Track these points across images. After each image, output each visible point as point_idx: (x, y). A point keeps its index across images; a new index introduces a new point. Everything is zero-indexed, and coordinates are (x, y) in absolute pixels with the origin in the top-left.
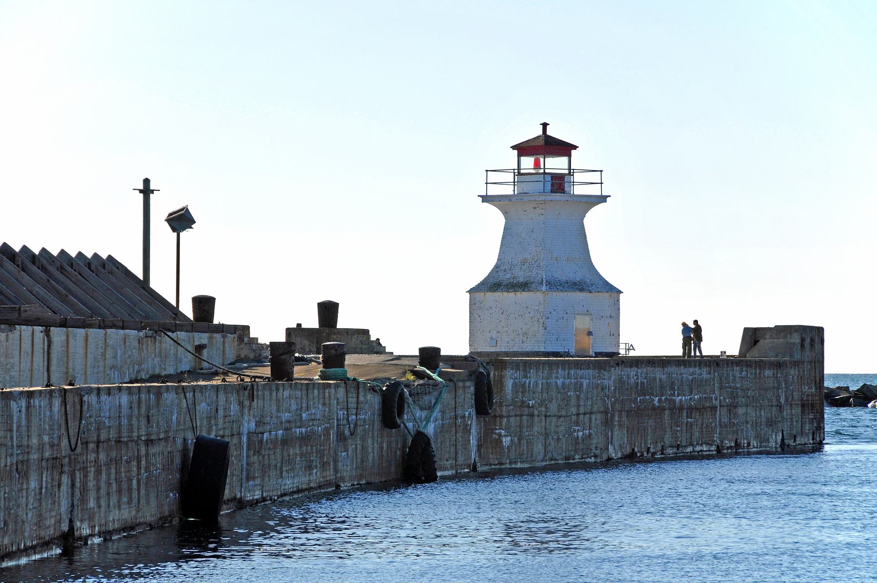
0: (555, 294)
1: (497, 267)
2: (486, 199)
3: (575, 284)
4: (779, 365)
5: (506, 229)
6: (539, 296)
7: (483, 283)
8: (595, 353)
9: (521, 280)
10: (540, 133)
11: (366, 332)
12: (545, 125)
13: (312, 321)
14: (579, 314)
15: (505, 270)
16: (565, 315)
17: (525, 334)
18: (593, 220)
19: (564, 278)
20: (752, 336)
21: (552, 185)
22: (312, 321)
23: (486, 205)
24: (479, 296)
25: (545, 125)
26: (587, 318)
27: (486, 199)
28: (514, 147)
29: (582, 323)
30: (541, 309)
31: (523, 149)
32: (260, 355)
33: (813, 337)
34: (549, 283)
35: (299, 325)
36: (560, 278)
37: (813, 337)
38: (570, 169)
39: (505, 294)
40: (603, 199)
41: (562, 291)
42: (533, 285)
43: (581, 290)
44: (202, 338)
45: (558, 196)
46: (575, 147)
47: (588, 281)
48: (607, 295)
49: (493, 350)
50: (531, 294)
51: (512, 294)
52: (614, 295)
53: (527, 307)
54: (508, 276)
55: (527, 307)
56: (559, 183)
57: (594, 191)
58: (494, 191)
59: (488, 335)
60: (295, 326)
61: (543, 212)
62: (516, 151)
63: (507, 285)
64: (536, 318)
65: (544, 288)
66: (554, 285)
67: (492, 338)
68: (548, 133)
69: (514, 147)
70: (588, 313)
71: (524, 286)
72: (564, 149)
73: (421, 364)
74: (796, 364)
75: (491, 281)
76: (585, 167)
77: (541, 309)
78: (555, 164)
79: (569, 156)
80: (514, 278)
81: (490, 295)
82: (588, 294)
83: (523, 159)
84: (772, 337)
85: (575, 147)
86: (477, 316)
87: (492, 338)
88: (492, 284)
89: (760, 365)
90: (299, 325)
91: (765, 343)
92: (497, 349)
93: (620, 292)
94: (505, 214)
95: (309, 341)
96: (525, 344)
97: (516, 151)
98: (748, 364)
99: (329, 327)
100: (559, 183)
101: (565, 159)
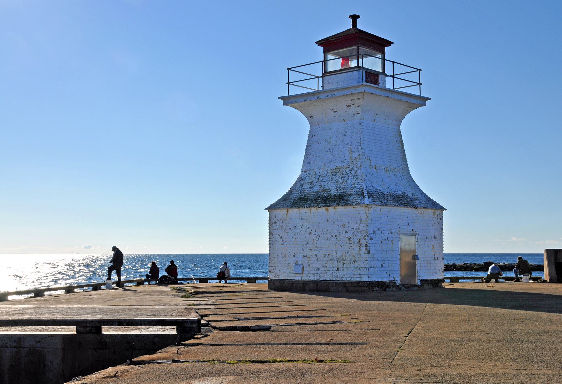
0: (379, 208)
1: (300, 179)
3: (398, 197)
5: (311, 136)
6: (360, 210)
7: (285, 198)
9: (333, 192)
12: (355, 18)
14: (404, 234)
15: (311, 183)
16: (390, 236)
18: (410, 125)
19: (385, 191)
23: (289, 109)
24: (281, 213)
25: (355, 18)
26: (413, 239)
27: (287, 100)
30: (363, 227)
31: (329, 45)
34: (370, 195)
36: (382, 190)
39: (314, 209)
41: (387, 205)
42: (351, 198)
43: (407, 205)
46: (389, 43)
47: (410, 195)
48: (430, 212)
49: (298, 278)
50: (350, 208)
51: (322, 210)
52: (438, 212)
53: (344, 226)
54: (316, 189)
55: (344, 226)
59: (292, 260)
61: (359, 110)
62: (322, 48)
63: (315, 200)
64: (355, 239)
65: (367, 200)
66: (379, 198)
67: (297, 264)
68: (216, 277)
69: (320, 43)
71: (339, 199)
72: (379, 45)
73: (488, 271)
75: (295, 195)
76: (397, 66)
77: (363, 227)
78: (372, 63)
79: (383, 53)
80: (323, 191)
81: (294, 211)
82: (415, 211)
85: (389, 43)
86: (278, 237)
87: (297, 264)
88: (296, 199)
92: (304, 277)
93: (443, 209)
94: (310, 118)
96: (341, 272)
97: (322, 48)
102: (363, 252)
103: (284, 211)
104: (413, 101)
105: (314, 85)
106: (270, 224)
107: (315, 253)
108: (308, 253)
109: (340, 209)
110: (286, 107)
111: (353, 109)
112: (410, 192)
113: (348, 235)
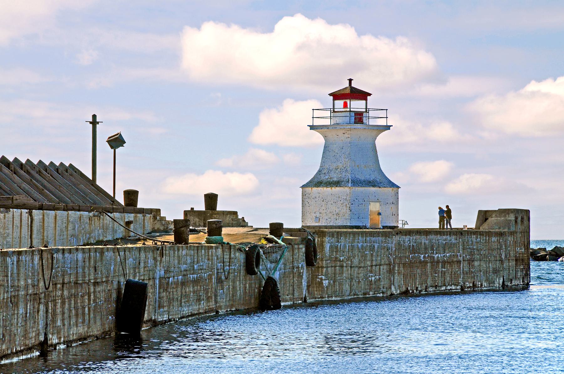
1: (320, 171)
2: (312, 127)
3: (370, 182)
4: (501, 234)
6: (347, 189)
7: (310, 182)
8: (383, 226)
9: (335, 179)
10: (348, 85)
11: (235, 213)
12: (350, 80)
13: (201, 206)
15: (325, 173)
17: (337, 214)
20: (484, 216)
21: (355, 119)
22: (201, 206)
24: (308, 190)
25: (350, 80)
26: (378, 204)
27: (312, 127)
28: (330, 95)
29: (374, 207)
31: (336, 96)
32: (167, 228)
33: (523, 216)
35: (192, 209)
37: (523, 216)
38: (366, 108)
39: (325, 188)
40: (388, 127)
41: (361, 187)
44: (130, 217)
45: (359, 126)
46: (370, 95)
47: (378, 180)
50: (342, 188)
51: (329, 189)
52: (395, 189)
54: (327, 177)
55: (339, 197)
56: (359, 117)
57: (382, 122)
58: (317, 122)
59: (314, 215)
60: (190, 209)
61: (349, 136)
62: (332, 97)
63: (326, 183)
66: (356, 183)
67: (316, 217)
69: (330, 95)
70: (378, 201)
71: (337, 184)
72: (363, 95)
73: (271, 234)
74: (512, 233)
75: (316, 180)
78: (357, 105)
79: (366, 100)
81: (315, 189)
83: (336, 102)
84: (496, 216)
85: (370, 95)
86: (307, 203)
87: (316, 217)
88: (316, 183)
89: (489, 234)
90: (192, 209)
91: (492, 220)
93: (398, 187)
94: (325, 137)
95: (199, 218)
96: (338, 221)
97: (332, 97)
98: (481, 234)
99: (211, 209)
100: (359, 117)
101: (364, 102)
102: (348, 211)
103: (310, 189)
104: (381, 128)
105: (327, 122)
106: (303, 195)
107: (325, 211)
108: (321, 211)
109: (338, 189)
110: (312, 130)
111: (346, 135)
112: (379, 178)
113: (341, 202)
